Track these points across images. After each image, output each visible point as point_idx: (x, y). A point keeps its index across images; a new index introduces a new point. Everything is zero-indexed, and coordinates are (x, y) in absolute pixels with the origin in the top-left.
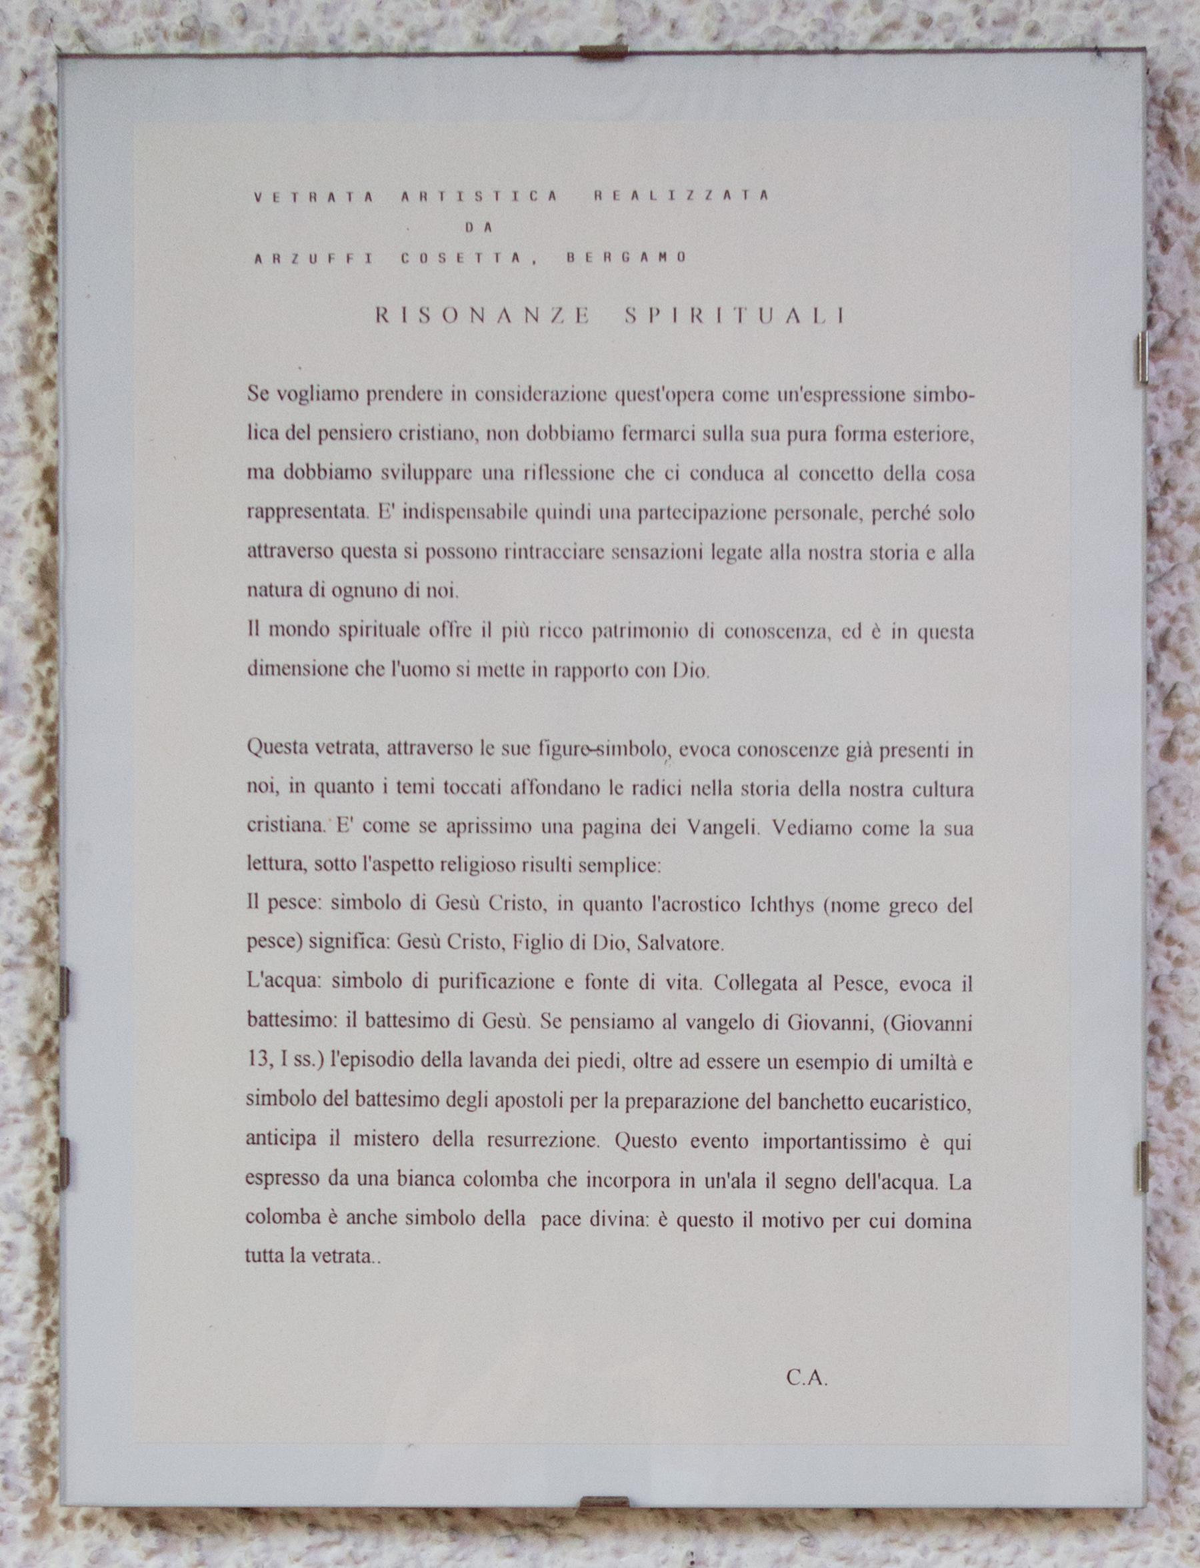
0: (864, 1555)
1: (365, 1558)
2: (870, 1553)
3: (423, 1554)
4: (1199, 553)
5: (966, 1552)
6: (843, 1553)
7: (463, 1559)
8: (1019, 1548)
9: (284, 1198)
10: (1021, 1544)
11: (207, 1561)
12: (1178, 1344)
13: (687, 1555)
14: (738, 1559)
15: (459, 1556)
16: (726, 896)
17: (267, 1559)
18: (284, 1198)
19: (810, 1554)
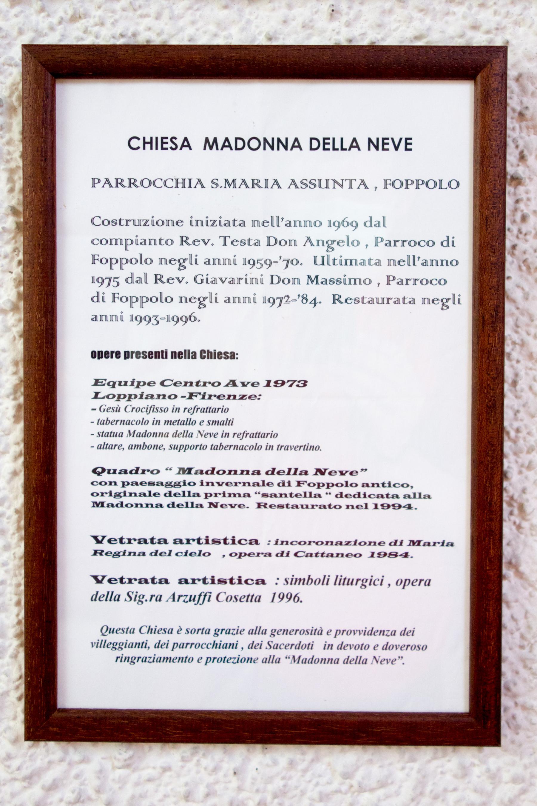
0: (434, 8)
1: (140, 7)
2: (438, 8)
3: (174, 7)
4: (536, 483)
5: (495, 7)
6: (422, 7)
7: (198, 10)
8: (526, 6)
9: (108, 428)
10: (527, 4)
11: (47, 9)
12: (525, 544)
13: (330, 6)
14: (360, 11)
15: (196, 7)
16: (288, 134)
17: (82, 7)
18: (108, 428)
19: (403, 7)
